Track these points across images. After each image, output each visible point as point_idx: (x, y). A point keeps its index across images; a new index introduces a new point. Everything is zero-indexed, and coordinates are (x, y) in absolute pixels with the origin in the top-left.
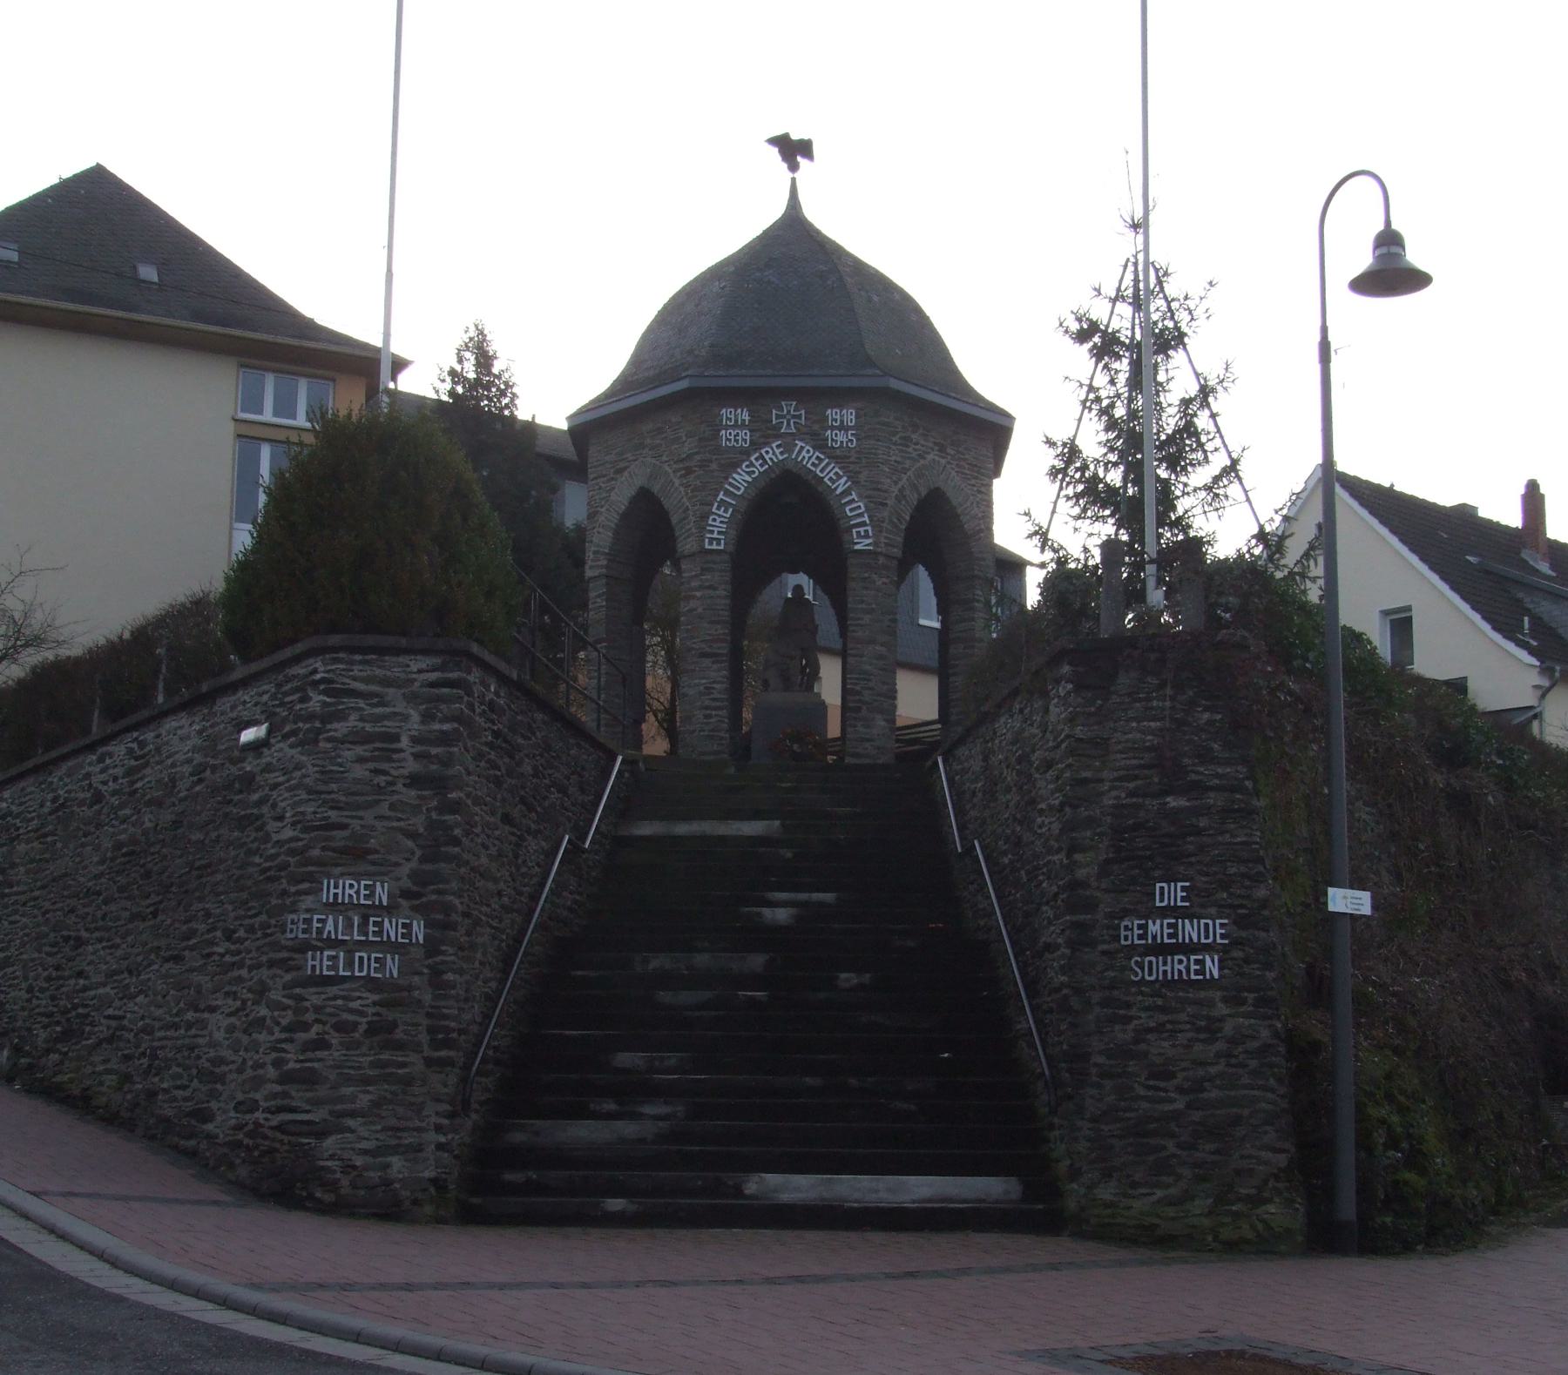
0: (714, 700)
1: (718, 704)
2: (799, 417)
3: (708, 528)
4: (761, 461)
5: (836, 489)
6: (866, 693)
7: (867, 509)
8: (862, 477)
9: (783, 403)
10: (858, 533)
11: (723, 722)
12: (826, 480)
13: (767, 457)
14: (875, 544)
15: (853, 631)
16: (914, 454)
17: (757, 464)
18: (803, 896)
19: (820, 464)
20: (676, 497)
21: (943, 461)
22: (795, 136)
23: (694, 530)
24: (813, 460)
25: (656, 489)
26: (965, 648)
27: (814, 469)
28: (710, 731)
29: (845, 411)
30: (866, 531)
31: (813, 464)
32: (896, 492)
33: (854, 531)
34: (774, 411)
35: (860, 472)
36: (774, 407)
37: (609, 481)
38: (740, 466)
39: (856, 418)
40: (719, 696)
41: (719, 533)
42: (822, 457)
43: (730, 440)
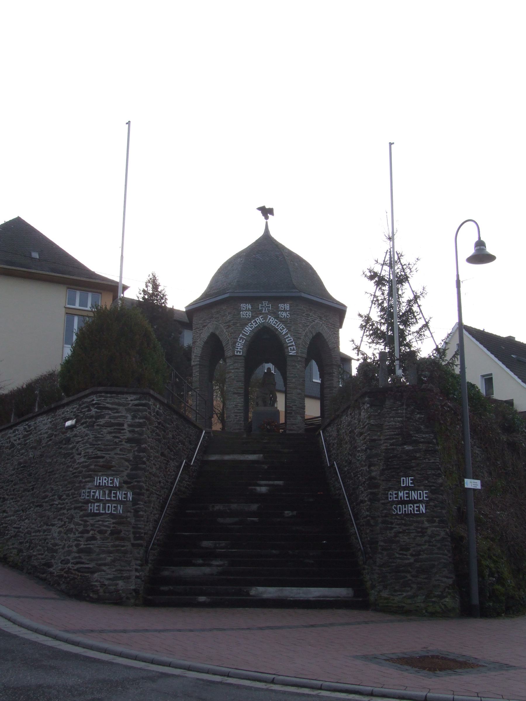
0: (239, 410)
1: (240, 411)
2: (269, 307)
4: (255, 323)
5: (283, 333)
6: (294, 407)
7: (294, 340)
8: (292, 329)
9: (263, 302)
11: (242, 418)
12: (279, 329)
13: (257, 321)
14: (297, 353)
15: (289, 384)
17: (254, 324)
18: (271, 482)
19: (276, 324)
20: (225, 336)
21: (321, 323)
22: (267, 207)
23: (231, 348)
24: (274, 322)
25: (217, 333)
28: (237, 421)
29: (285, 305)
30: (294, 348)
31: (274, 324)
32: (304, 334)
33: (289, 348)
34: (260, 305)
35: (291, 327)
36: (260, 304)
37: (200, 330)
38: (248, 325)
39: (289, 307)
40: (240, 408)
41: (240, 349)
42: (277, 321)
43: (244, 315)
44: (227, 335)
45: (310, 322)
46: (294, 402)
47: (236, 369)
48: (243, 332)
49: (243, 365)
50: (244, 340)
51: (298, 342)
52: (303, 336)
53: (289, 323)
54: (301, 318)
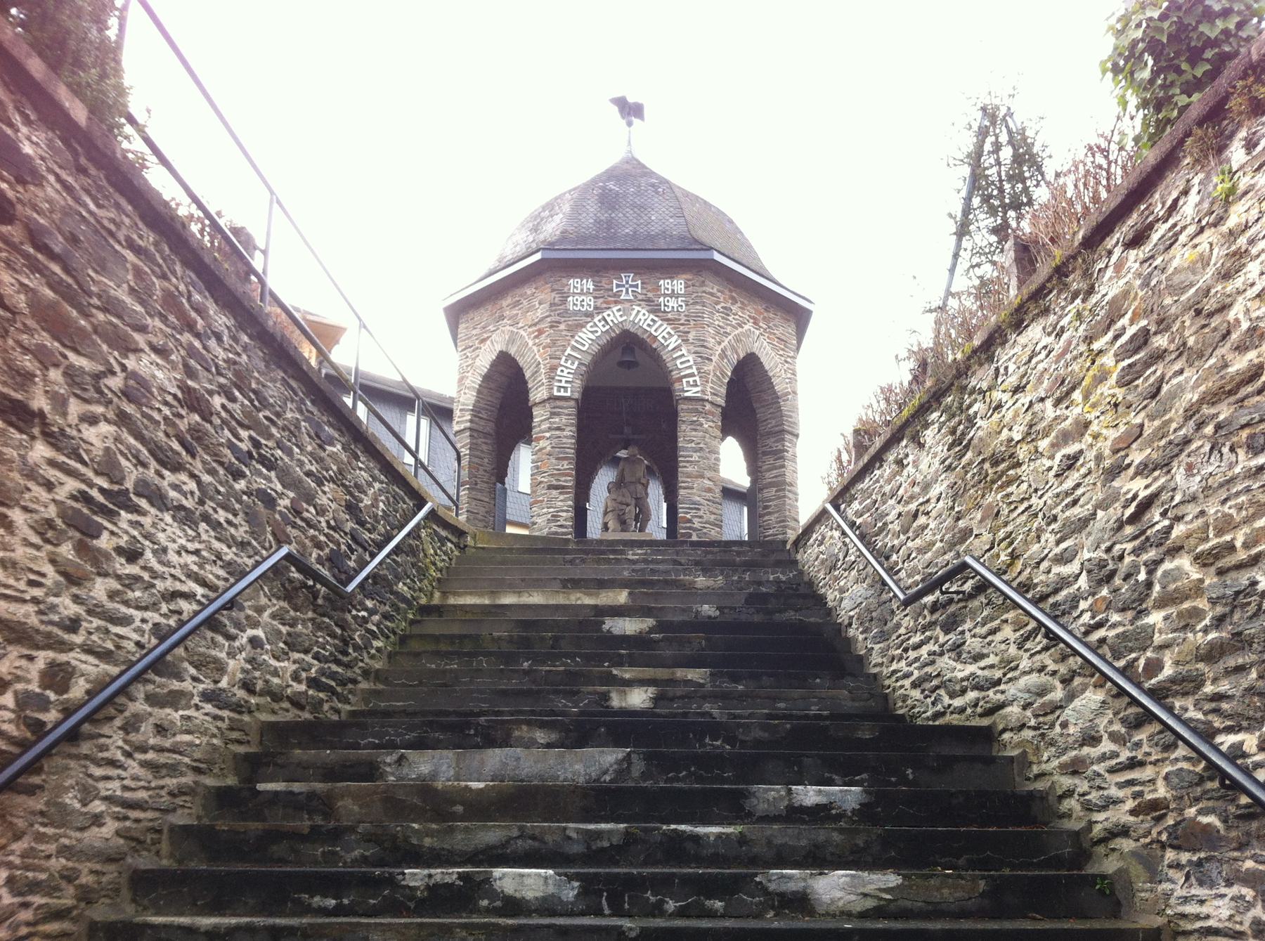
0: (561, 526)
2: (636, 286)
3: (557, 378)
7: (695, 363)
8: (691, 337)
10: (688, 382)
12: (659, 338)
13: (608, 319)
14: (703, 392)
16: (734, 322)
17: (600, 325)
18: (661, 673)
20: (532, 357)
21: (757, 332)
22: (631, 100)
23: (544, 381)
26: (776, 491)
27: (648, 329)
29: (675, 282)
31: (649, 325)
33: (684, 380)
34: (615, 282)
40: (564, 523)
41: (566, 382)
42: (656, 319)
45: (733, 327)
46: (695, 509)
47: (558, 429)
50: (576, 363)
51: (706, 368)
53: (682, 324)
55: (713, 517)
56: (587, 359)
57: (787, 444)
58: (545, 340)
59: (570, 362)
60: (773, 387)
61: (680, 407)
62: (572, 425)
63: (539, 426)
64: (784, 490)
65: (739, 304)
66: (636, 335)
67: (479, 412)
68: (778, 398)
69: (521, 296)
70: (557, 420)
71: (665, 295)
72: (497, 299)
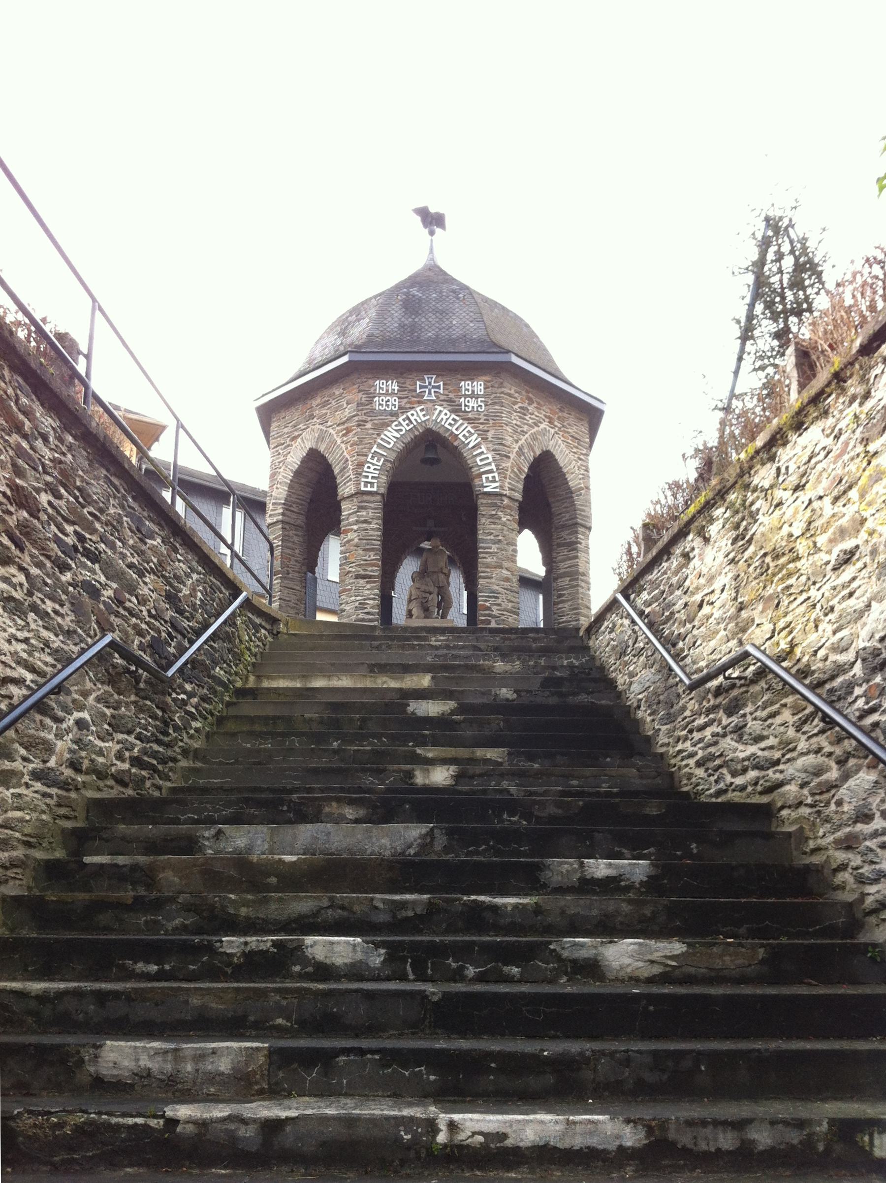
0: (368, 613)
3: (364, 474)
5: (468, 443)
7: (494, 460)
8: (490, 435)
9: (426, 377)
10: (487, 478)
12: (460, 436)
13: (412, 418)
14: (501, 487)
15: (485, 558)
17: (404, 424)
21: (552, 431)
22: (432, 210)
23: (352, 476)
24: (450, 421)
25: (322, 448)
26: (570, 581)
29: (475, 383)
31: (450, 424)
32: (517, 449)
33: (484, 476)
34: (418, 383)
36: (419, 380)
37: (285, 448)
40: (371, 610)
41: (373, 478)
42: (457, 418)
43: (382, 405)
44: (344, 448)
47: (365, 522)
48: (379, 441)
49: (377, 591)
50: (382, 460)
51: (504, 465)
52: (515, 454)
53: (482, 424)
54: (509, 412)
55: (510, 605)
56: (392, 456)
57: (580, 536)
58: (352, 438)
59: (376, 459)
60: (567, 483)
61: (480, 501)
62: (378, 518)
63: (348, 519)
64: (577, 579)
65: (535, 405)
66: (438, 433)
67: (291, 506)
68: (572, 493)
69: (330, 396)
70: (364, 514)
71: (466, 396)
72: (307, 399)
